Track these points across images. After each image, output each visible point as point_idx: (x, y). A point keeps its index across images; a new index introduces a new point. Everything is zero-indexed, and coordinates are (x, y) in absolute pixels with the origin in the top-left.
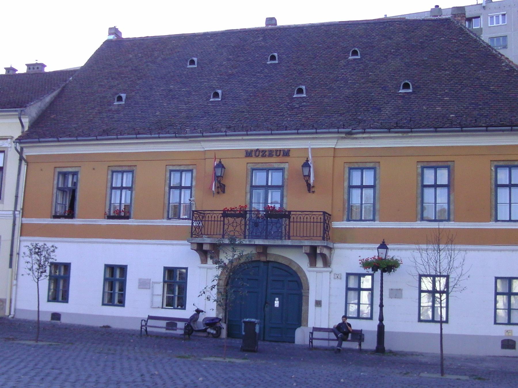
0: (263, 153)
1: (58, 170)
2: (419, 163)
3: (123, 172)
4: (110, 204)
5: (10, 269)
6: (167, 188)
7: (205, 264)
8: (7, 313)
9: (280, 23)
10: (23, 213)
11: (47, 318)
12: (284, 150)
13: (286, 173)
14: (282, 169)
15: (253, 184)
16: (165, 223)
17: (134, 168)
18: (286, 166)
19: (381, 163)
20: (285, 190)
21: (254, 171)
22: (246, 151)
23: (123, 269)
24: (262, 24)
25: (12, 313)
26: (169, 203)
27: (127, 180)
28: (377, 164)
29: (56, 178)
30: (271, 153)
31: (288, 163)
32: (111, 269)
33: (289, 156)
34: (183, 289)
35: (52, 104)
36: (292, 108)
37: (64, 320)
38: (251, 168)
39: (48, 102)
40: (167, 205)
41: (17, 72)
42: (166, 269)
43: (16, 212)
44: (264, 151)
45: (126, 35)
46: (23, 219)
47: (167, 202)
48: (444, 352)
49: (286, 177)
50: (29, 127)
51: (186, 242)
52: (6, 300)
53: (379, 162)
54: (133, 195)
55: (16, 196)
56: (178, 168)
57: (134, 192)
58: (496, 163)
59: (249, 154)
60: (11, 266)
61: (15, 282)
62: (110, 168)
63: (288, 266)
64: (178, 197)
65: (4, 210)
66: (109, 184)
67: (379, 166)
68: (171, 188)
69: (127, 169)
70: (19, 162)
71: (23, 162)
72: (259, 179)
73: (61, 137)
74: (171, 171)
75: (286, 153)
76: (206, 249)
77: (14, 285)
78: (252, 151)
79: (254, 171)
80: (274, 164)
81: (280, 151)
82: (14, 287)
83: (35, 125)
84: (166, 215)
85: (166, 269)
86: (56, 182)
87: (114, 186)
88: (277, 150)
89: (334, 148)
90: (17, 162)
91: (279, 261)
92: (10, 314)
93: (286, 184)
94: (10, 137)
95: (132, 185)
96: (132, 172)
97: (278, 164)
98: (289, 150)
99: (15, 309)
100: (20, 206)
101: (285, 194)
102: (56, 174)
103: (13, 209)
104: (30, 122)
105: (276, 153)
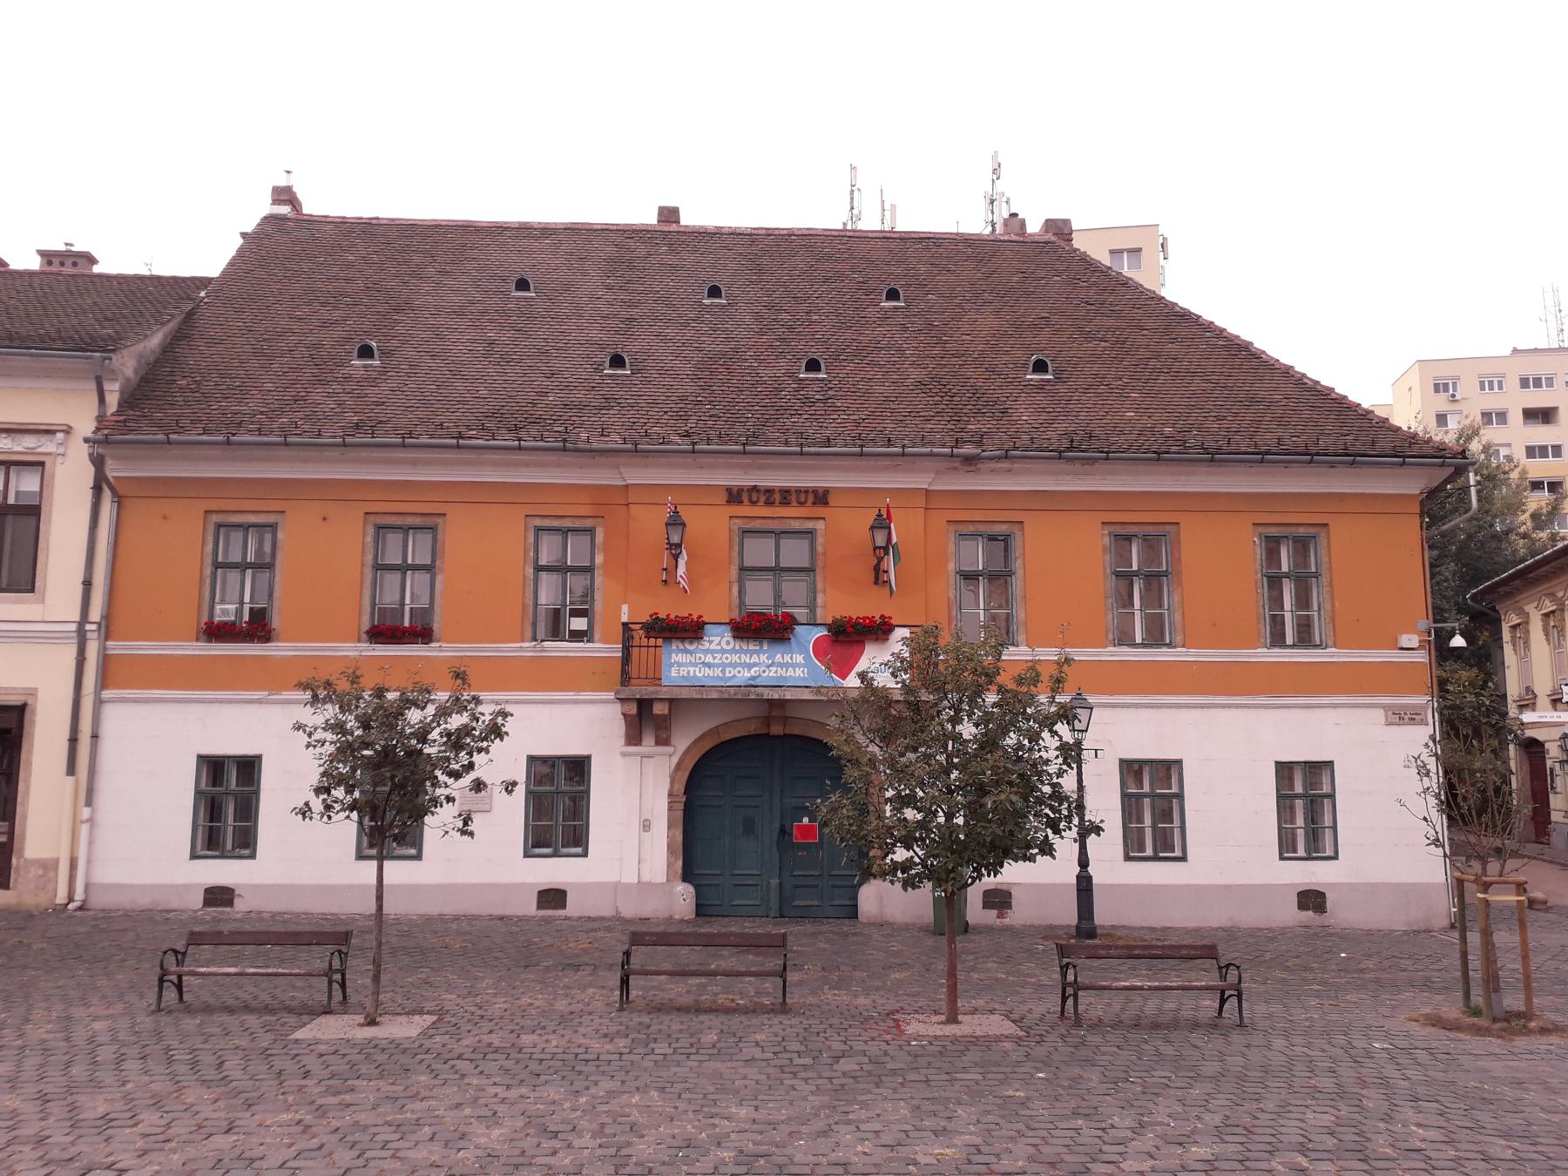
0: (769, 496)
1: (215, 518)
2: (1107, 527)
3: (406, 530)
4: (373, 604)
5: (70, 778)
6: (530, 571)
7: (636, 745)
8: (61, 897)
9: (688, 219)
10: (107, 628)
11: (1289, 914)
12: (815, 491)
13: (820, 540)
14: (810, 533)
15: (569, 564)
16: (526, 648)
17: (440, 520)
18: (820, 525)
19: (1331, 526)
20: (819, 579)
21: (222, 529)
22: (729, 490)
23: (249, 767)
24: (650, 218)
25: (79, 895)
26: (536, 604)
27: (418, 550)
28: (1017, 527)
29: (210, 539)
30: (786, 497)
31: (824, 518)
32: (213, 767)
33: (828, 503)
34: (248, 809)
35: (168, 349)
36: (807, 401)
37: (573, 908)
38: (739, 529)
39: (152, 352)
40: (531, 609)
41: (96, 269)
42: (202, 759)
43: (88, 627)
44: (769, 491)
45: (312, 206)
46: (110, 643)
47: (530, 602)
48: (388, 908)
49: (820, 549)
50: (120, 405)
51: (611, 696)
52: (56, 862)
53: (1178, 523)
54: (439, 586)
55: (83, 583)
56: (556, 523)
57: (439, 579)
58: (538, 522)
59: (734, 496)
60: (71, 769)
61: (86, 813)
62: (371, 518)
63: (722, 743)
64: (398, 588)
65: (46, 619)
66: (369, 558)
67: (1022, 530)
68: (539, 569)
69: (418, 521)
70: (93, 494)
71: (107, 495)
72: (760, 552)
73: (234, 435)
74: (539, 529)
75: (821, 498)
76: (659, 712)
77: (82, 822)
78: (741, 490)
79: (222, 529)
80: (792, 522)
81: (806, 492)
82: (85, 828)
83: (130, 400)
84: (529, 633)
85: (202, 759)
86: (209, 547)
87: (220, 559)
88: (799, 491)
89: (927, 491)
90: (88, 496)
91: (727, 737)
92: (71, 899)
93: (820, 564)
94: (64, 428)
95: (433, 561)
96: (432, 529)
97: (802, 521)
98: (827, 491)
99: (87, 887)
100: (96, 613)
101: (820, 586)
102: (211, 529)
103: (77, 618)
104: (122, 392)
105: (798, 497)
